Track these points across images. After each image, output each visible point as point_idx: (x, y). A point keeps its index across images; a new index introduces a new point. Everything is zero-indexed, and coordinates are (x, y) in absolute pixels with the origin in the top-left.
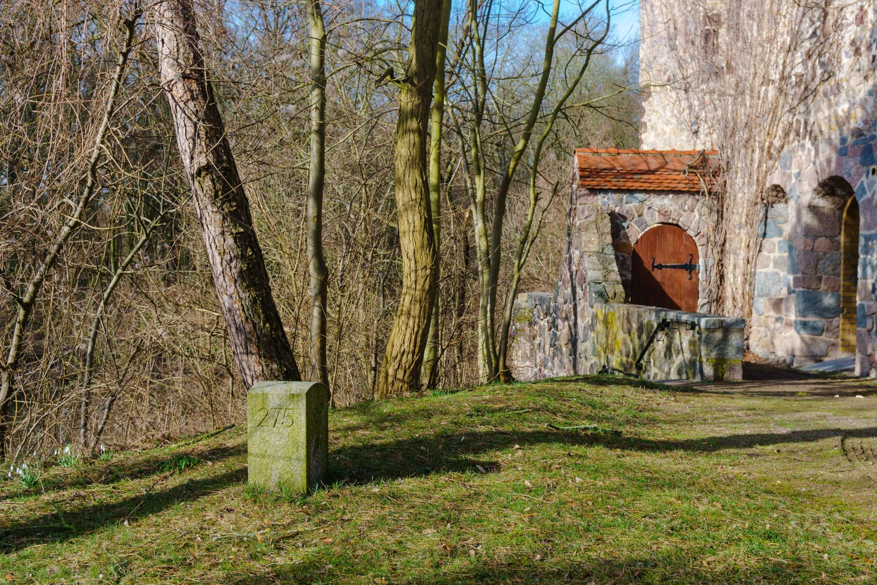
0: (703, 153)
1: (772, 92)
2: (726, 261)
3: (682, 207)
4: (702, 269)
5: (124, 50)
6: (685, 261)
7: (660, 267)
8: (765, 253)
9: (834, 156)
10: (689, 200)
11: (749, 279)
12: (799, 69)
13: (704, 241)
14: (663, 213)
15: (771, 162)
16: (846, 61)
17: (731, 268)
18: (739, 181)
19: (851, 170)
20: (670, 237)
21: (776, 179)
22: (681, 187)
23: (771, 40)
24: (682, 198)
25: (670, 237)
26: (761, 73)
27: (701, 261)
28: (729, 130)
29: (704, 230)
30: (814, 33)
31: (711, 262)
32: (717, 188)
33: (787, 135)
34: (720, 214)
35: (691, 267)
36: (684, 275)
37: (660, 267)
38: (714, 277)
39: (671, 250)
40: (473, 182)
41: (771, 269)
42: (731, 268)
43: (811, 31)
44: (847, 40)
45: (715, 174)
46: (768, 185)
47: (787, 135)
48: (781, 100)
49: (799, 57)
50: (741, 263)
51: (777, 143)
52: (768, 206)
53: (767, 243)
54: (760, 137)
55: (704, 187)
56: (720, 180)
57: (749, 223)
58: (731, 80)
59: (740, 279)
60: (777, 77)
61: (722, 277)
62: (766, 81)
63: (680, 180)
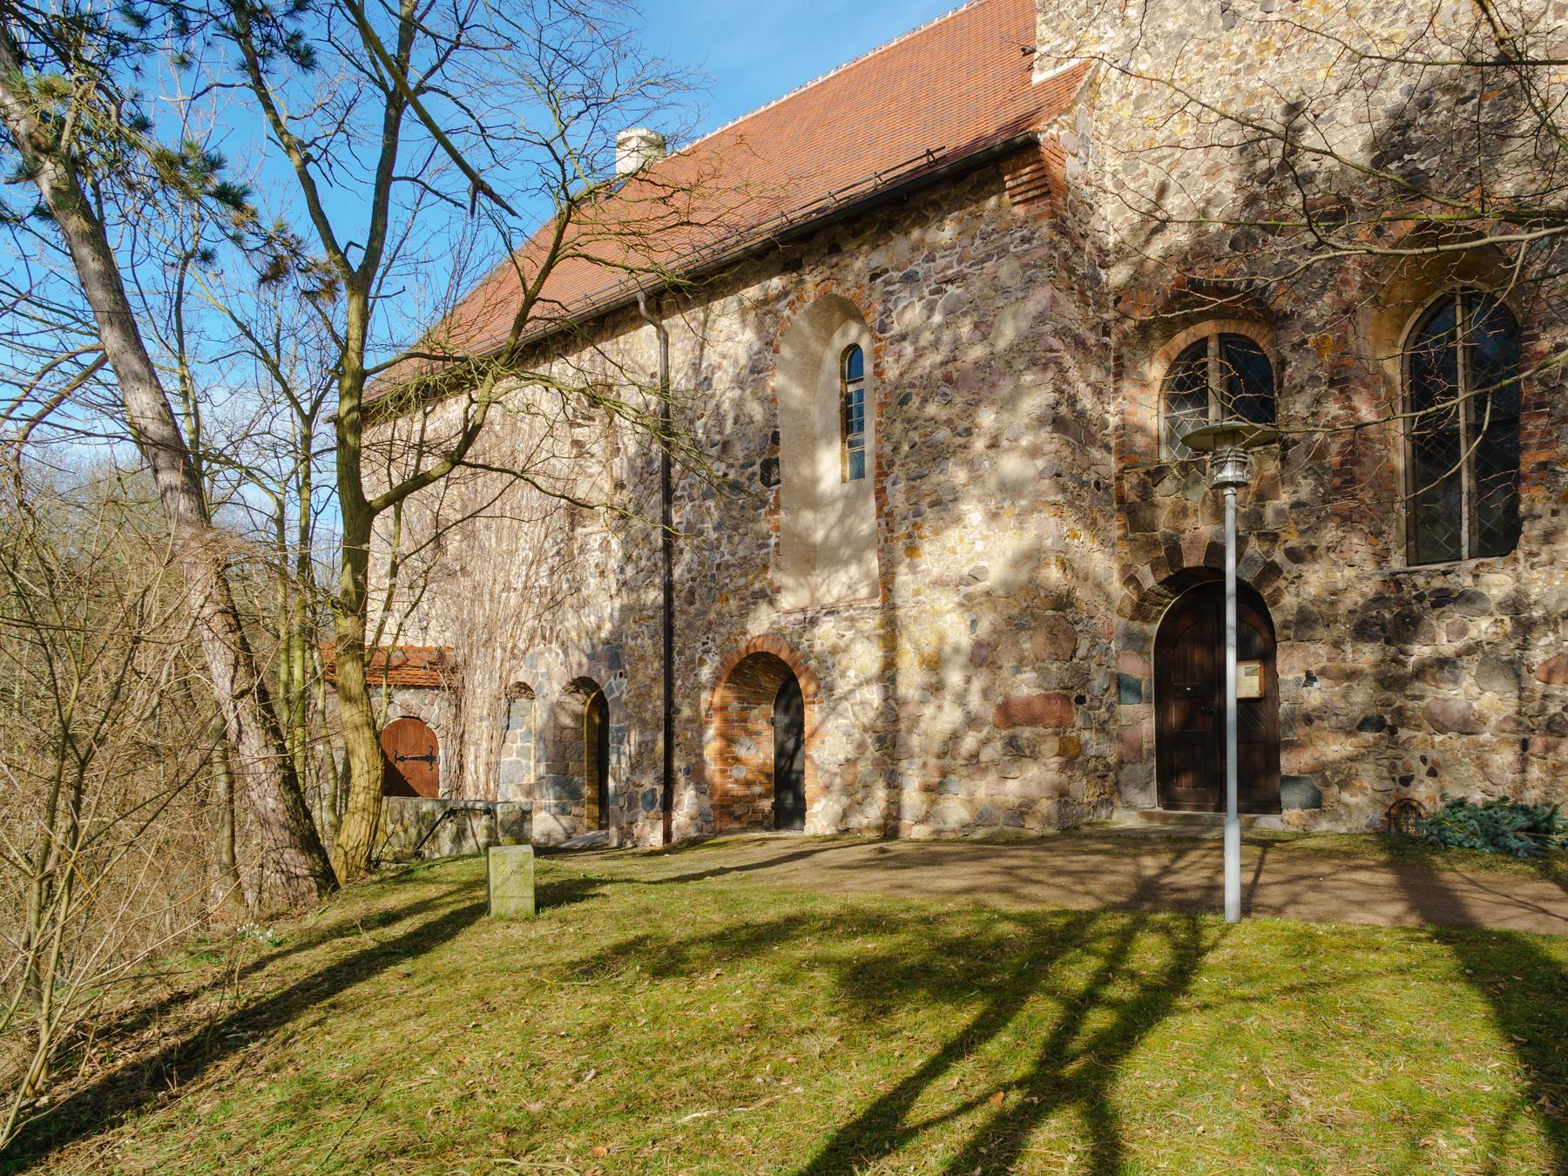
0: (439, 650)
1: (514, 599)
2: (465, 752)
3: (422, 701)
4: (442, 760)
5: (58, 502)
6: (426, 753)
7: (403, 759)
8: (508, 743)
9: (585, 660)
10: (431, 694)
11: (493, 767)
12: (544, 582)
13: (443, 733)
14: (407, 707)
15: (514, 662)
16: (593, 582)
17: (472, 757)
18: (478, 676)
19: (603, 676)
20: (411, 729)
21: (522, 676)
22: (421, 682)
23: (512, 553)
24: (421, 694)
25: (411, 729)
26: (500, 580)
27: (441, 752)
28: (467, 628)
29: (443, 722)
30: (558, 553)
31: (450, 753)
32: (455, 684)
33: (532, 639)
34: (458, 707)
35: (431, 759)
36: (426, 765)
37: (403, 759)
38: (454, 764)
39: (413, 742)
40: (1383, 915)
41: (514, 758)
42: (472, 757)
43: (555, 549)
44: (592, 562)
45: (453, 670)
46: (512, 682)
47: (532, 639)
48: (525, 606)
49: (544, 570)
50: (483, 753)
51: (522, 646)
52: (511, 701)
53: (510, 734)
54: (501, 637)
55: (444, 683)
56: (459, 676)
57: (492, 714)
58: (465, 582)
59: (482, 769)
60: (520, 586)
61: (461, 767)
62: (508, 588)
63: (421, 676)
